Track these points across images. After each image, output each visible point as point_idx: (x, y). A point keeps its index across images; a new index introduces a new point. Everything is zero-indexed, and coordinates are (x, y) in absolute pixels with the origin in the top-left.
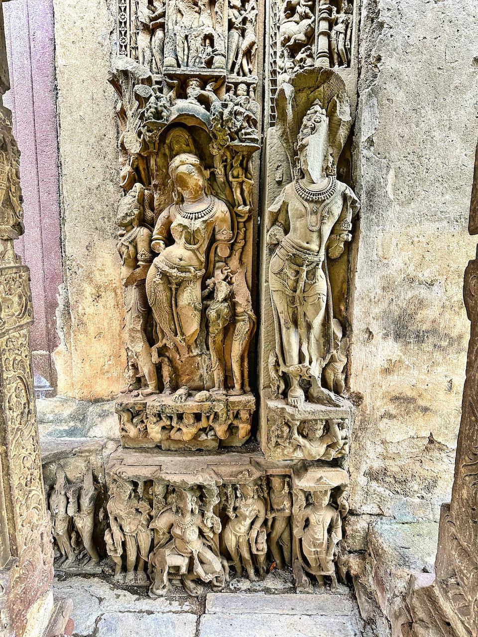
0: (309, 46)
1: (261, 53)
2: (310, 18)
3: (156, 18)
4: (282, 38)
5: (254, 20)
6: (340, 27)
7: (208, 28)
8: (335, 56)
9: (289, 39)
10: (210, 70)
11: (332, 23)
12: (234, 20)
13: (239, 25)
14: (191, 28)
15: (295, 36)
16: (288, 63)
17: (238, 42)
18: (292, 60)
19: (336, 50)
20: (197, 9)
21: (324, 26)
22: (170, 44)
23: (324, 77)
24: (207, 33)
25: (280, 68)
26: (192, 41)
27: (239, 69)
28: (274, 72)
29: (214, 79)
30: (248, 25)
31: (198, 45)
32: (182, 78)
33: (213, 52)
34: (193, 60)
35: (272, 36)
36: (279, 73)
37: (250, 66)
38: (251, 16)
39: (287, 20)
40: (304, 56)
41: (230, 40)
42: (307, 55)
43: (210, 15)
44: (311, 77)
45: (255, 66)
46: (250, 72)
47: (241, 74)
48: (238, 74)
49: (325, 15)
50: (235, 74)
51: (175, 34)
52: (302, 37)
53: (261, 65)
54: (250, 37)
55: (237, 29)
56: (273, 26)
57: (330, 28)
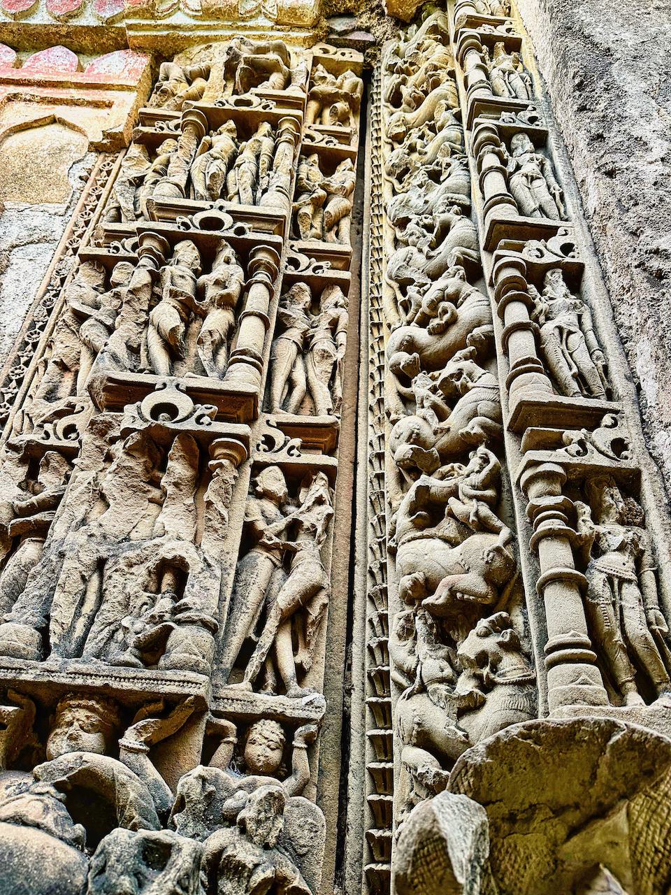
0: (504, 614)
1: (341, 614)
2: (496, 531)
3: (32, 509)
4: (406, 582)
5: (320, 530)
6: (615, 562)
7: (175, 544)
8: (621, 660)
9: (428, 586)
10: (148, 673)
11: (586, 551)
12: (261, 525)
13: (276, 540)
14: (127, 539)
15: (449, 578)
16: (432, 664)
17: (270, 582)
18: (442, 653)
19: (618, 636)
20: (156, 493)
21: (556, 557)
22: (41, 580)
23: (632, 768)
24: (169, 556)
25: (399, 668)
26: (116, 576)
27: (263, 666)
28: (380, 679)
29: (160, 706)
30: (303, 541)
31: (133, 587)
32: (42, 693)
33: (175, 611)
34: (105, 633)
35: (371, 621)
36: (401, 688)
37: (303, 656)
38: (313, 518)
39: (419, 534)
40: (490, 644)
41: (243, 577)
42: (501, 644)
43: (193, 511)
44: (563, 763)
45: (317, 658)
46: (301, 673)
47: (270, 679)
48: (258, 684)
49: (557, 524)
50: (246, 685)
51: (62, 555)
52: (474, 583)
53: (339, 646)
54: (307, 570)
55: (268, 548)
56: (376, 547)
57: (581, 562)
